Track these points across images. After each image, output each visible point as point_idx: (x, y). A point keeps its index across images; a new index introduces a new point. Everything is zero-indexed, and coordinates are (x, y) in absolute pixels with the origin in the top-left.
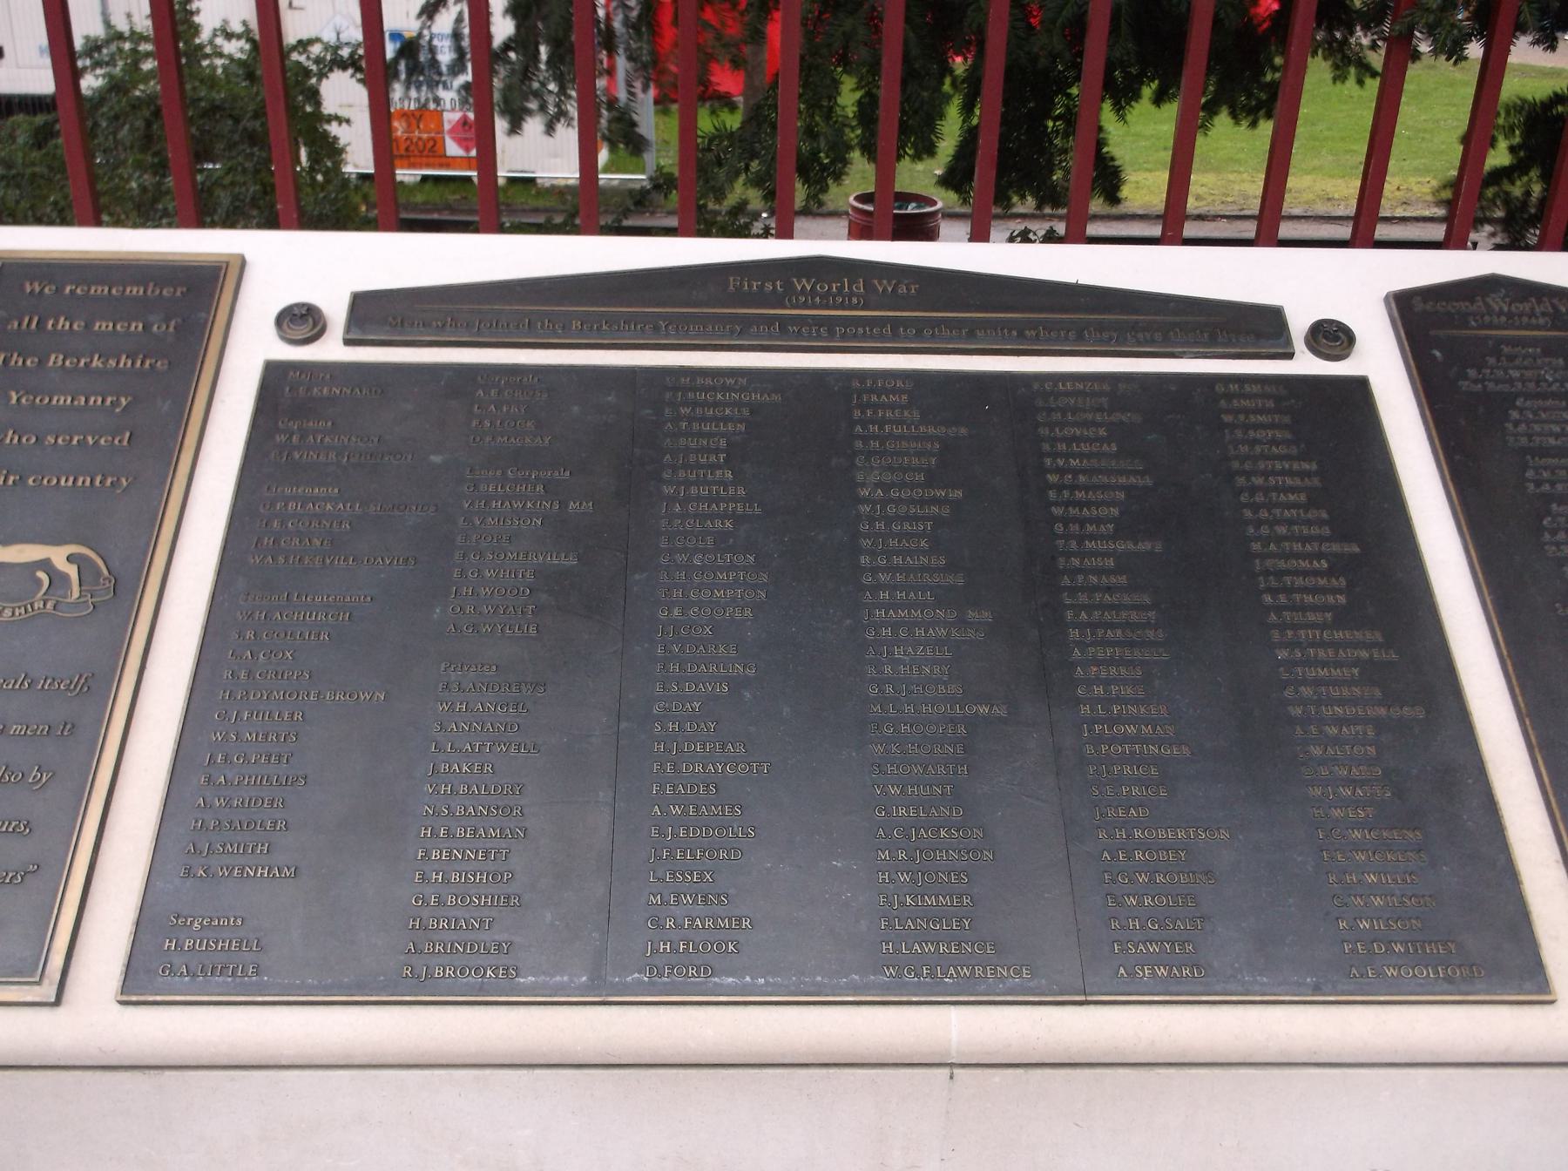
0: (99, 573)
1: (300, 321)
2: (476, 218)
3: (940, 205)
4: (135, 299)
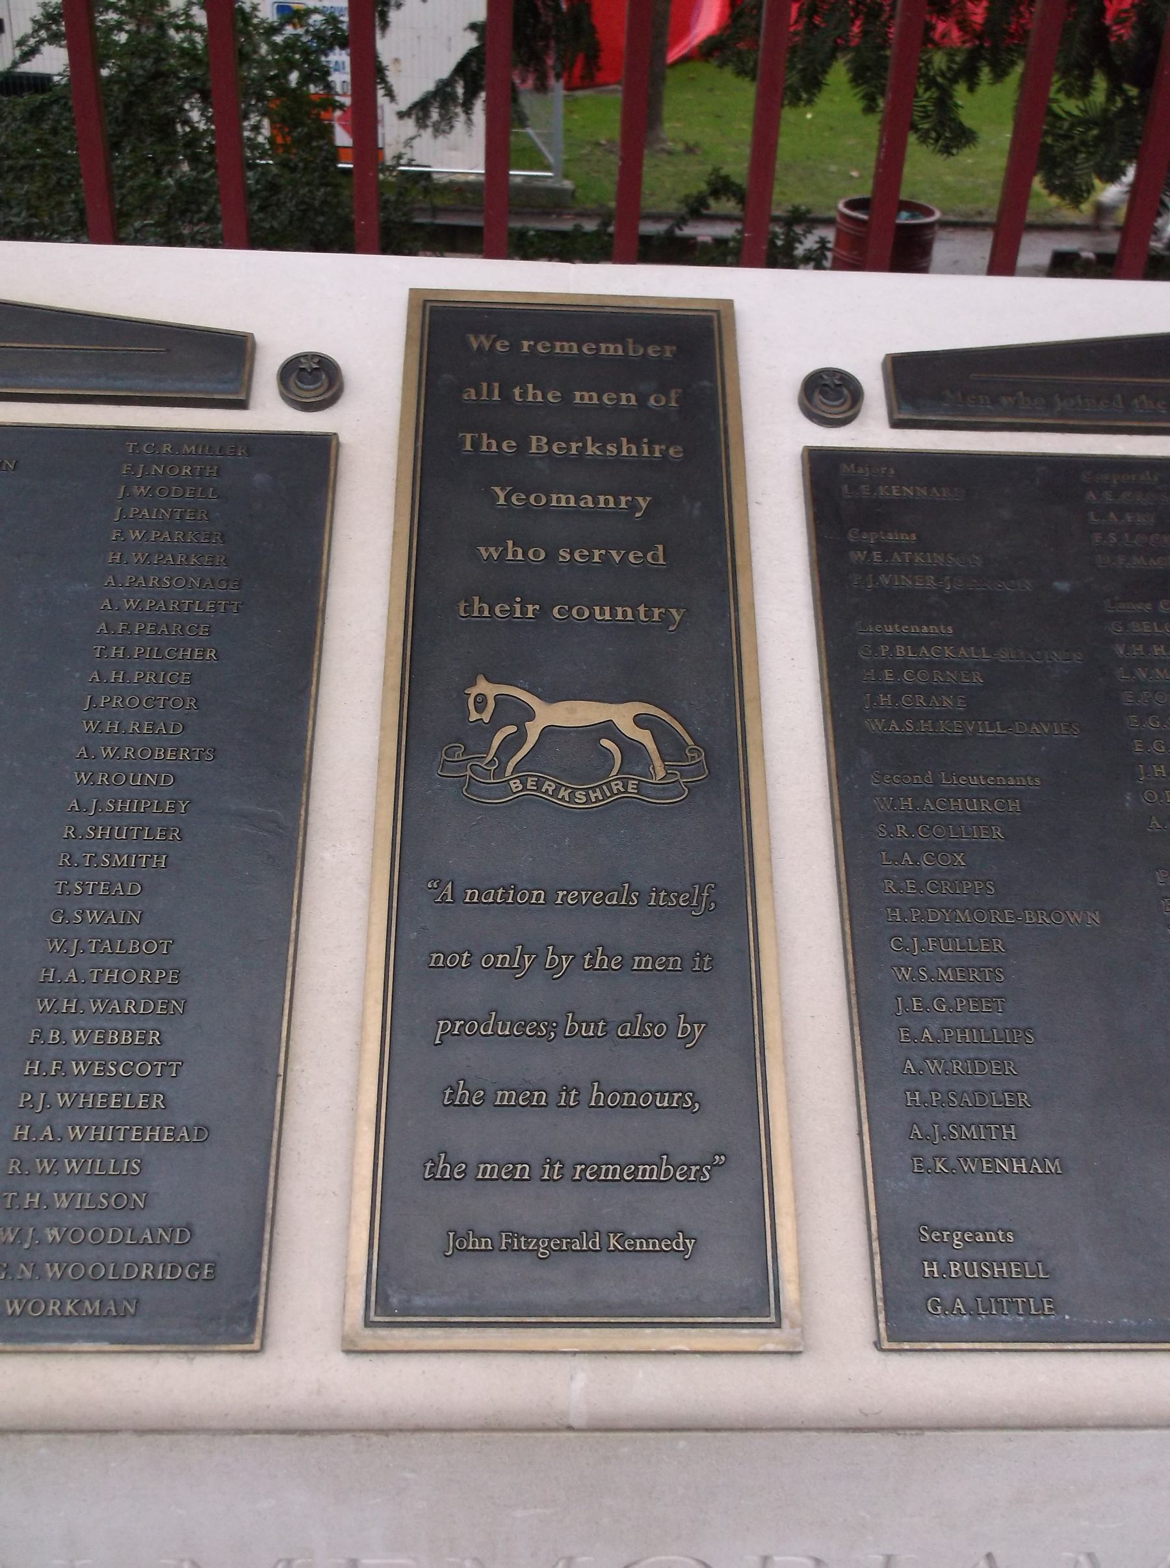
0: (682, 746)
1: (829, 394)
2: (476, 221)
3: (937, 215)
4: (612, 359)
